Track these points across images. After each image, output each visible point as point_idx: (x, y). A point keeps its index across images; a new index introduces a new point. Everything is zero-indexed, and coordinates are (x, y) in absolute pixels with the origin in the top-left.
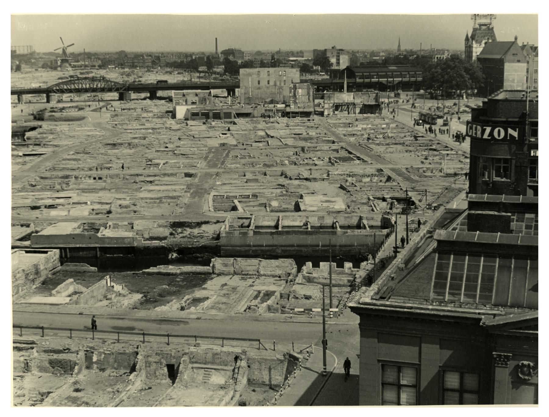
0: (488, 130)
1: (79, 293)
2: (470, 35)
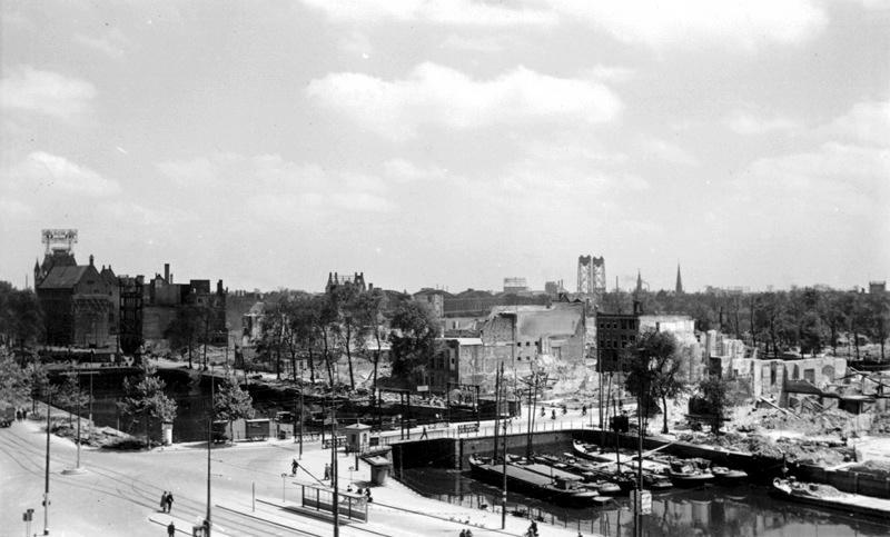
2: (41, 264)
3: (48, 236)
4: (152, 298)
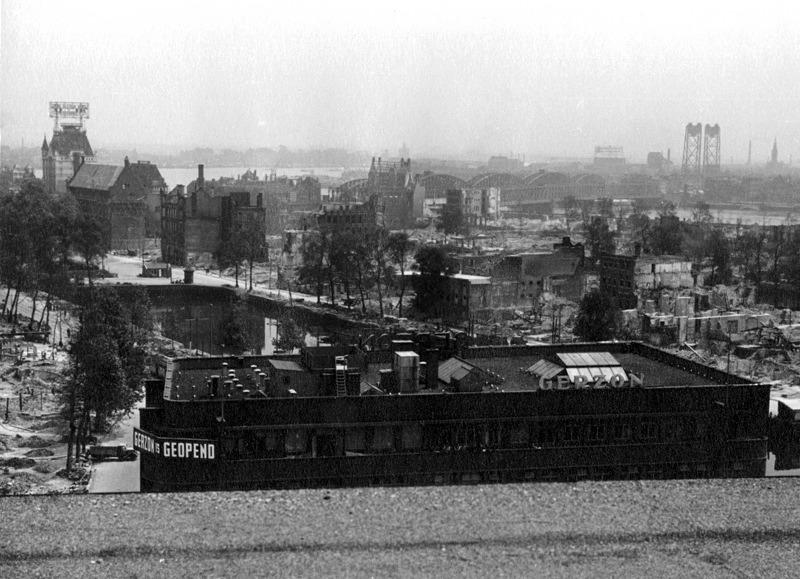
1: (684, 288)
2: (49, 140)
3: (56, 109)
4: (194, 211)
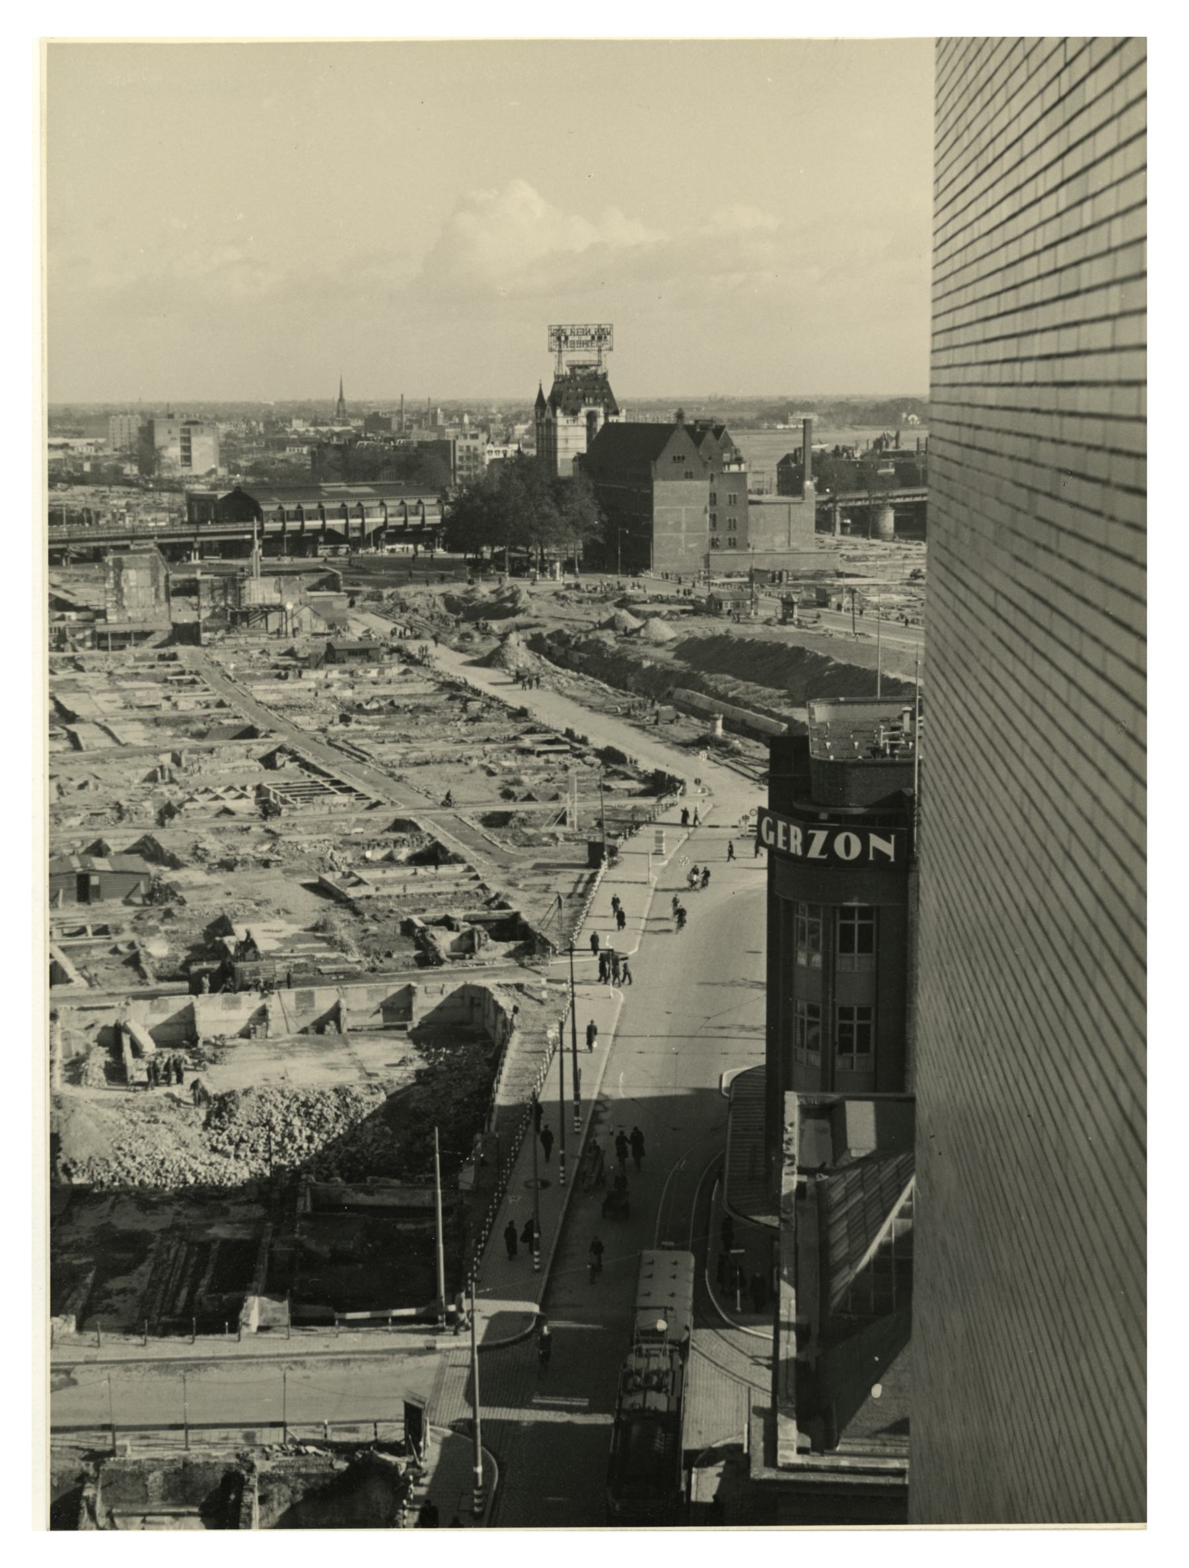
0: (820, 837)
2: (547, 394)
